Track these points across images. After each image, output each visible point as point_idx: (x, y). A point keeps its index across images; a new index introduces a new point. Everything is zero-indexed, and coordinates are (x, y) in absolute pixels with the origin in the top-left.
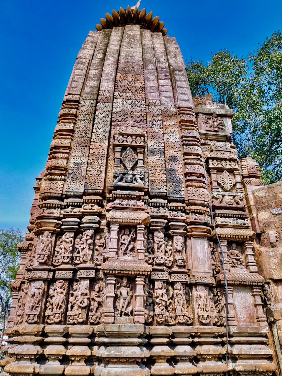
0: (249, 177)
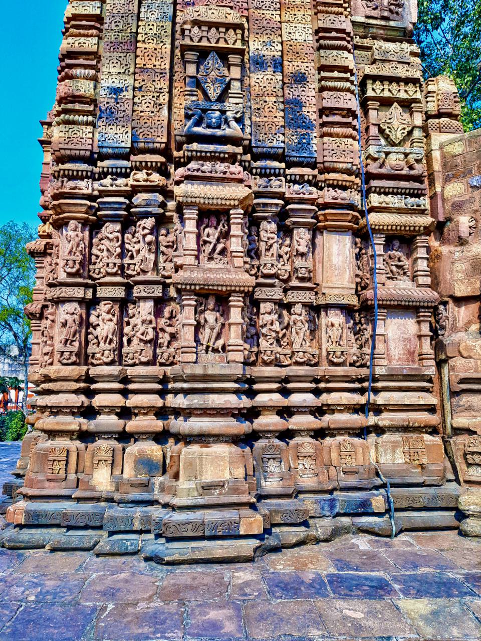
0: (439, 115)
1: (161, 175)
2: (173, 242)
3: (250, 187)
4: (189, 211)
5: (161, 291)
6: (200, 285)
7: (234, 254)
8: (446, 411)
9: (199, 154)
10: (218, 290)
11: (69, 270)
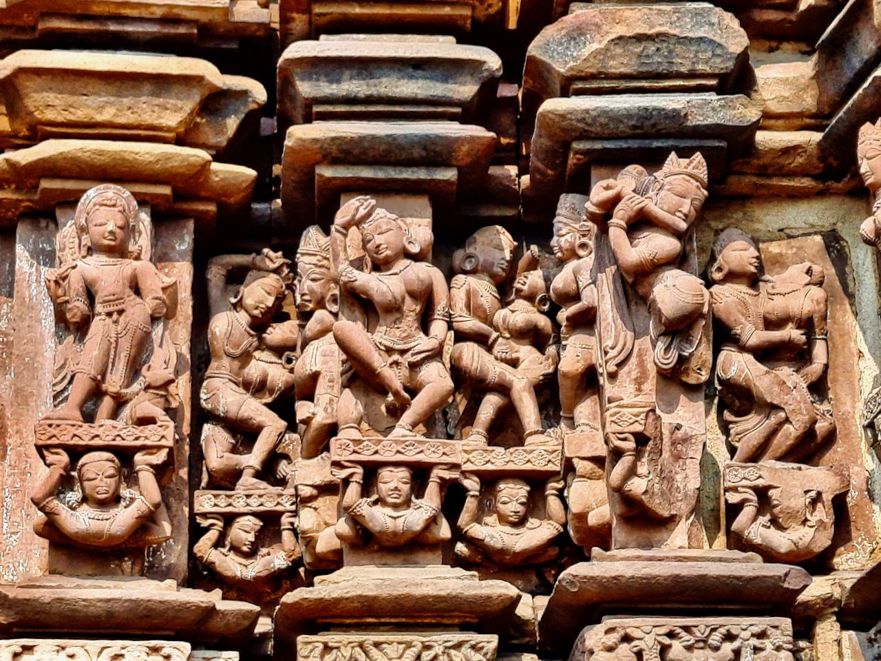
11: (80, 520)
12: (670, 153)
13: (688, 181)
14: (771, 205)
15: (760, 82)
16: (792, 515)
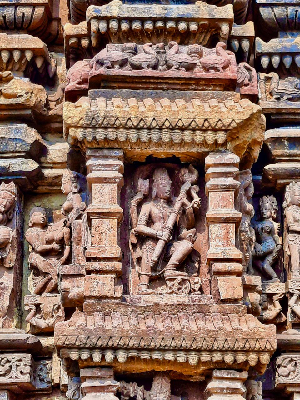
1: (33, 80)
2: (61, 242)
3: (254, 99)
4: (100, 162)
5: (28, 369)
6: (127, 349)
7: (217, 266)
8: (92, 380)
9: (125, 26)
10: (175, 362)
12: (2, 182)
13: (6, 193)
14: (57, 196)
15: (50, 151)
16: (48, 314)
